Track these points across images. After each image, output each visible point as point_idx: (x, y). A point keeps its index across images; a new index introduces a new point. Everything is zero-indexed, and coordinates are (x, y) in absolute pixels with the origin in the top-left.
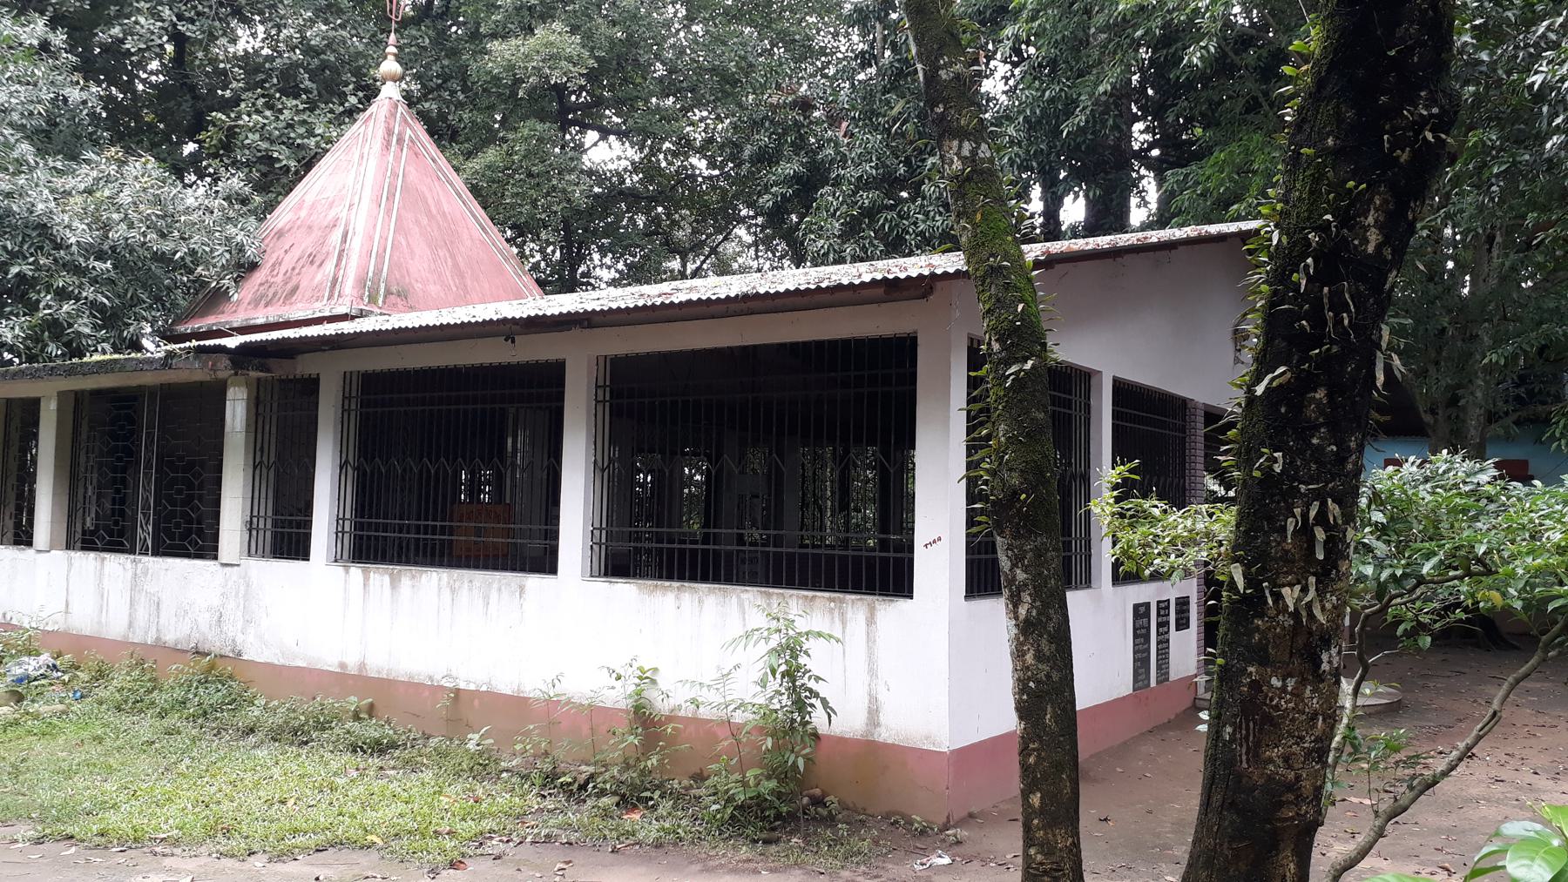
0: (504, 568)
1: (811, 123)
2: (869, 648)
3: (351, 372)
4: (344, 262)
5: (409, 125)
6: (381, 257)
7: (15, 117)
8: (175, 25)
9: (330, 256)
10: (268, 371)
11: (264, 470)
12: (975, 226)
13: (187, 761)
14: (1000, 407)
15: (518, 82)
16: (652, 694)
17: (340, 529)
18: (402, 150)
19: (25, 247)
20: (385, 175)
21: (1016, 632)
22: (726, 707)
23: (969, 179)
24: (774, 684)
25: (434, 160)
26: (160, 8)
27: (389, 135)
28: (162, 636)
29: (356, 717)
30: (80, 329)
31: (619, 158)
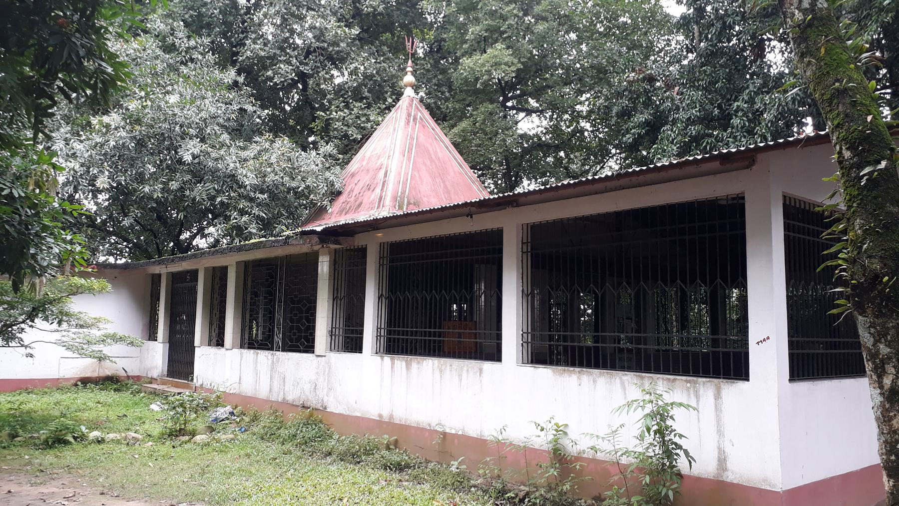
0: (470, 358)
1: (655, 89)
2: (717, 416)
3: (384, 243)
4: (385, 188)
5: (420, 111)
6: (405, 184)
7: (221, 120)
8: (298, 67)
9: (378, 185)
10: (340, 244)
11: (339, 302)
12: (819, 60)
13: (292, 471)
14: (855, 205)
15: (477, 79)
16: (566, 442)
17: (379, 334)
18: (416, 124)
19: (224, 188)
20: (406, 139)
21: (882, 399)
22: (616, 453)
23: (810, 25)
24: (649, 439)
25: (433, 129)
26: (291, 59)
27: (409, 117)
28: (286, 398)
29: (388, 448)
30: (251, 230)
31: (538, 127)
